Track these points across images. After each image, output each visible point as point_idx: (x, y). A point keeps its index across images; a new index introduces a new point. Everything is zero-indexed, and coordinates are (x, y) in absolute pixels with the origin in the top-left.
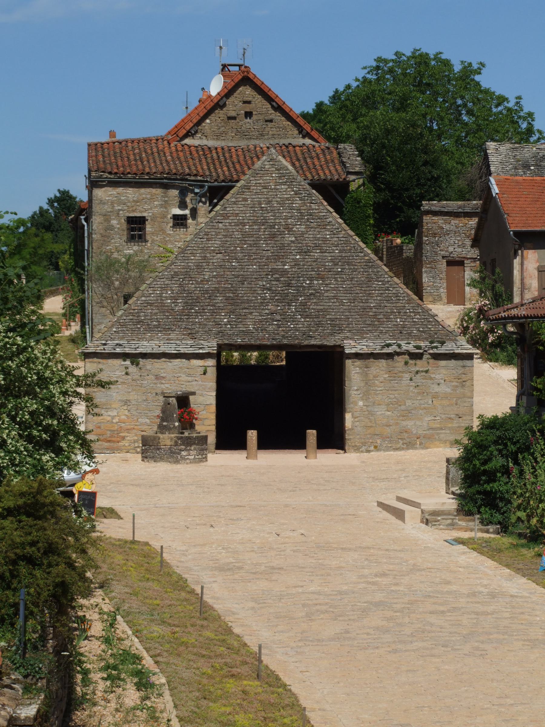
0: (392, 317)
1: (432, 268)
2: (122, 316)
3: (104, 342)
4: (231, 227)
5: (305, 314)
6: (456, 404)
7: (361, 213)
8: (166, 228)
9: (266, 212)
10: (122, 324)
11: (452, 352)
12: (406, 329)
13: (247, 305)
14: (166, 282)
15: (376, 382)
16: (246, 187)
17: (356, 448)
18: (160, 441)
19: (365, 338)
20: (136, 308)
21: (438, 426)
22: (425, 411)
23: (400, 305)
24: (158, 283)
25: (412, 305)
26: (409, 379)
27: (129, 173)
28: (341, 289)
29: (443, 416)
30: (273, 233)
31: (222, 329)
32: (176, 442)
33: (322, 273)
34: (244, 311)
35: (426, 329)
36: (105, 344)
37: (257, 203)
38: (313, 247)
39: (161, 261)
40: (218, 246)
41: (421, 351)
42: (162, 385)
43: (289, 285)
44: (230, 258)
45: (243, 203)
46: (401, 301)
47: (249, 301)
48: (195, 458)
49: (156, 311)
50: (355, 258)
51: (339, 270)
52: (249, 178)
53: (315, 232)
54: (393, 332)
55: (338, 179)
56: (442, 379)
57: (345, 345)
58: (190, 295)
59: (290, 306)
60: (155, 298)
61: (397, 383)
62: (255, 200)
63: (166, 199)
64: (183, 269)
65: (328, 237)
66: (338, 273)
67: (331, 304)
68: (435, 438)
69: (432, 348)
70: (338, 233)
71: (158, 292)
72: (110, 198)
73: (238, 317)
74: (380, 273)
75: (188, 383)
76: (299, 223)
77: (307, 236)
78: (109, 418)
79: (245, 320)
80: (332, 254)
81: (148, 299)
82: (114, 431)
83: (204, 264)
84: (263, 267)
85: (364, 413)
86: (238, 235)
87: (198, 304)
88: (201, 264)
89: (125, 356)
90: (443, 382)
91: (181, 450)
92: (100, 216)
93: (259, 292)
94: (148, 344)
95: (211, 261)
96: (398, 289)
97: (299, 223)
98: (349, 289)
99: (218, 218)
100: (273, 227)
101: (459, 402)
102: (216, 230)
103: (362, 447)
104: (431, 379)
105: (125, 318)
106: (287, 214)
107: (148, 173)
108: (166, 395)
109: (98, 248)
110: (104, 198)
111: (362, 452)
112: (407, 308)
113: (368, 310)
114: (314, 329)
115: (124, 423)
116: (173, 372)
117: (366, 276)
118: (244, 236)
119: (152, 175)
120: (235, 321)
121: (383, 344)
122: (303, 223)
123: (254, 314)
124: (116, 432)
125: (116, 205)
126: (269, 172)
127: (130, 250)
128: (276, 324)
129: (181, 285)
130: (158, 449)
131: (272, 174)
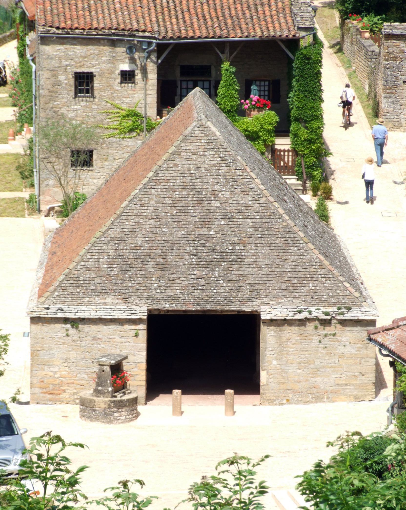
0: (305, 282)
1: (392, 93)
2: (63, 280)
3: (47, 306)
4: (162, 193)
5: (227, 279)
6: (360, 363)
7: (311, 69)
8: (113, 83)
9: (194, 178)
10: (63, 288)
11: (356, 318)
12: (317, 294)
13: (176, 270)
14: (103, 248)
15: (289, 343)
16: (177, 153)
17: (270, 401)
18: (96, 403)
19: (279, 303)
20: (76, 272)
21: (344, 382)
22: (332, 369)
23: (313, 270)
24: (96, 248)
25: (323, 270)
26: (318, 341)
27: (77, 28)
28: (260, 254)
29: (348, 374)
30: (200, 199)
31: (152, 294)
32: (109, 405)
33: (243, 239)
34: (173, 276)
35: (335, 294)
36: (48, 309)
37: (186, 169)
38: (236, 213)
39: (109, 117)
40: (151, 211)
41: (329, 317)
42: (99, 345)
43: (213, 251)
44: (161, 223)
45: (174, 169)
46: (314, 267)
47: (177, 266)
48: (126, 419)
49: (94, 276)
50: (274, 223)
51: (260, 236)
52: (180, 144)
53: (239, 199)
54: (305, 297)
55: (287, 36)
56: (347, 341)
57: (262, 310)
58: (124, 260)
59: (214, 271)
60: (93, 263)
61: (307, 345)
62: (185, 166)
63: (114, 55)
64: (119, 234)
65: (250, 203)
66: (258, 239)
67: (250, 269)
68: (341, 393)
69: (339, 314)
70: (260, 199)
71: (96, 257)
72: (58, 53)
73: (167, 282)
74: (296, 239)
75: (121, 344)
76: (224, 189)
77: (231, 202)
78: (52, 374)
79: (173, 285)
80: (253, 220)
81: (87, 263)
82: (56, 385)
83: (138, 230)
84: (191, 233)
85: (278, 371)
86: (168, 201)
87: (131, 269)
88: (134, 230)
89: (66, 320)
90: (349, 344)
91: (113, 412)
92: (48, 71)
93: (187, 257)
94: (86, 309)
95: (144, 227)
96: (311, 254)
97: (224, 189)
98: (267, 255)
99: (151, 184)
100: (200, 193)
101: (363, 361)
102: (149, 196)
103: (275, 400)
104: (338, 341)
105: (66, 282)
106: (213, 180)
107: (96, 29)
108: (101, 363)
109: (46, 104)
110: (51, 53)
111: (276, 404)
112: (318, 273)
113: (283, 275)
114: (234, 294)
115: (65, 378)
116: (108, 334)
117: (284, 242)
118: (174, 202)
119: (100, 30)
120: (164, 286)
121: (295, 310)
122: (228, 190)
123: (181, 279)
124: (57, 386)
125: (63, 60)
126: (198, 138)
127: (77, 106)
128: (201, 289)
129: (116, 251)
130: (94, 411)
131: (201, 140)
